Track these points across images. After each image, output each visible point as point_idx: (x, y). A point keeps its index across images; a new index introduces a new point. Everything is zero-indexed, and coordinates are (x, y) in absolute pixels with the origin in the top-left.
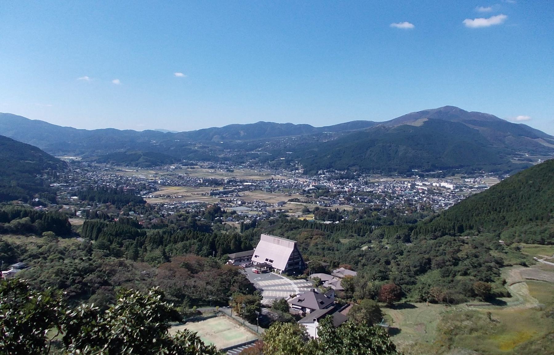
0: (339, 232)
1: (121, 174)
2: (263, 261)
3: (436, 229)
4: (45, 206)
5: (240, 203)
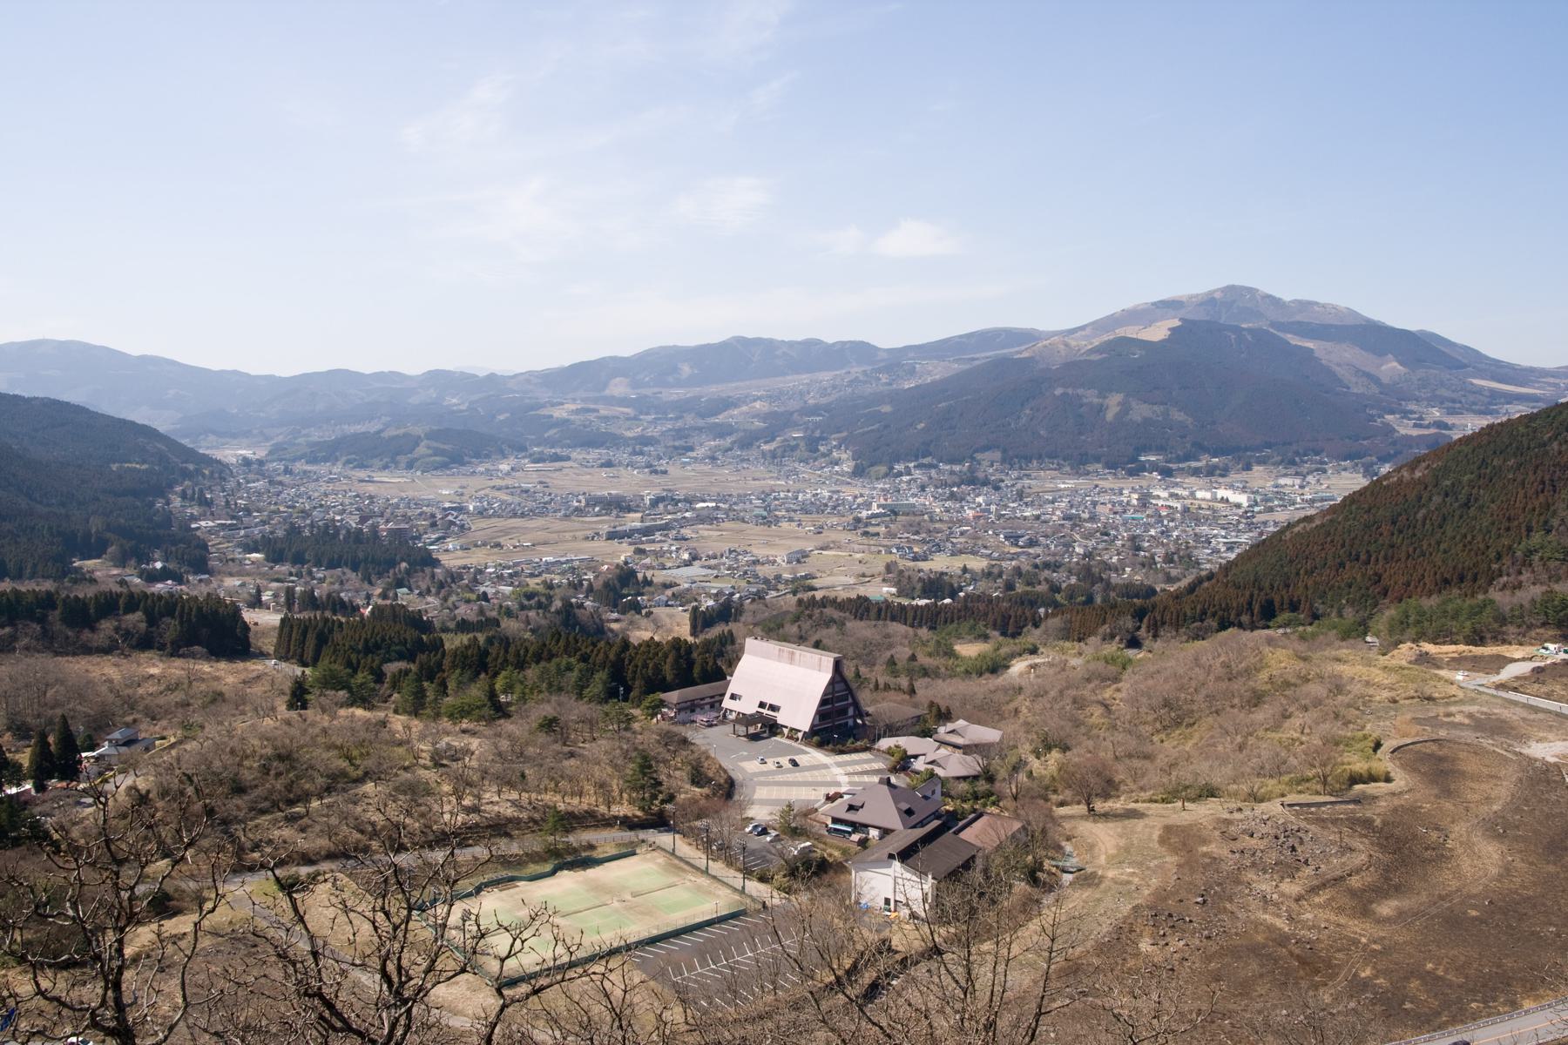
2: (749, 707)
3: (1204, 612)
4: (179, 580)
5: (686, 556)
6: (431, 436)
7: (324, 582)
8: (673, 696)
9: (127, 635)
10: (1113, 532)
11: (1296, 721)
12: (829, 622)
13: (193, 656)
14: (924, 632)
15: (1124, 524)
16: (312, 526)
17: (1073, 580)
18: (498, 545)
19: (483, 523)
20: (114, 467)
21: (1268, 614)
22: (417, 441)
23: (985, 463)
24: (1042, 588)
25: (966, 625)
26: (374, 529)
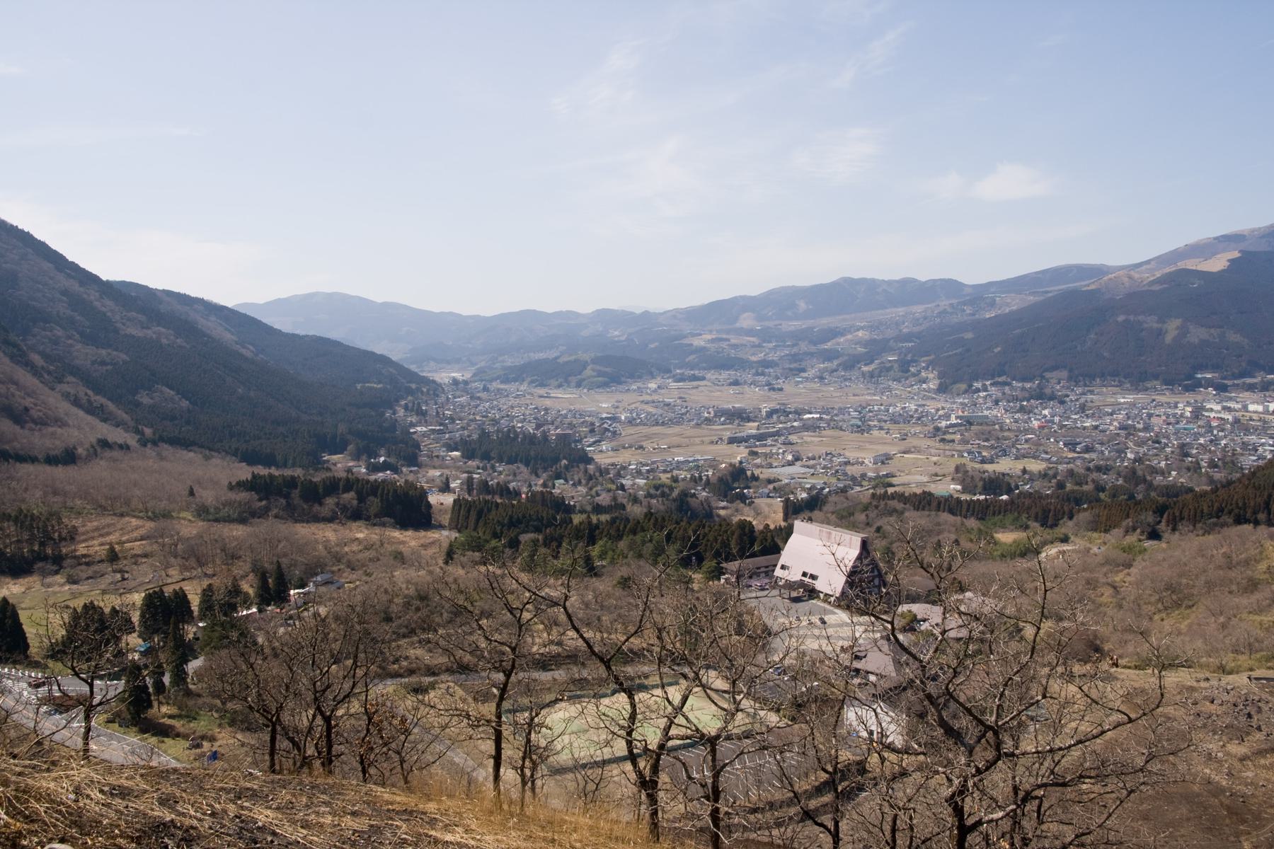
0: (996, 518)
1: (548, 403)
2: (795, 576)
3: (1221, 510)
4: (395, 470)
5: (790, 457)
6: (595, 361)
7: (501, 474)
8: (733, 566)
9: (344, 509)
10: (1164, 441)
12: (893, 511)
13: (384, 525)
14: (972, 523)
15: (1175, 434)
16: (498, 431)
17: (1120, 482)
18: (641, 447)
19: (631, 430)
20: (359, 386)
25: (1010, 517)
26: (545, 436)
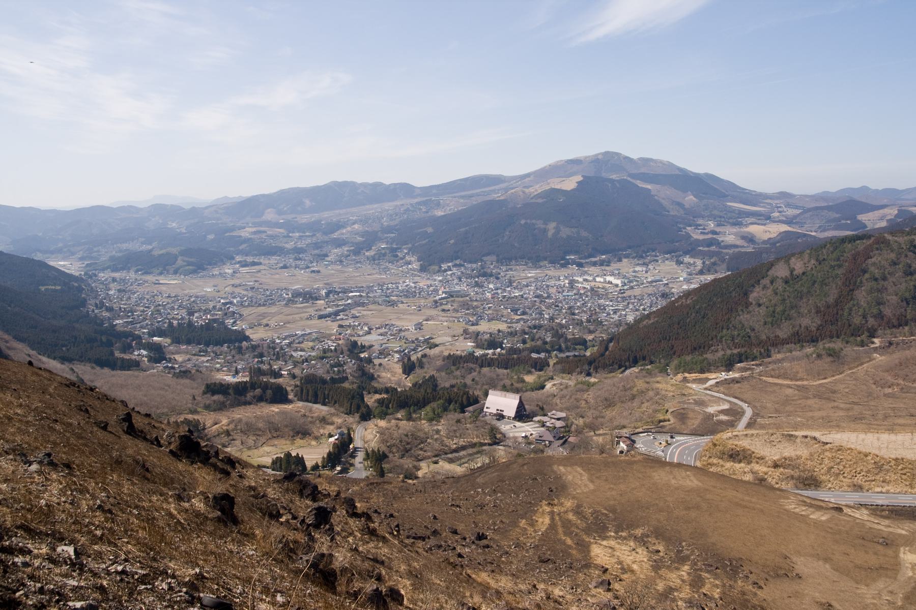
6: (183, 253)
11: (646, 404)
21: (635, 362)
22: (176, 258)
23: (488, 263)
24: (539, 343)
